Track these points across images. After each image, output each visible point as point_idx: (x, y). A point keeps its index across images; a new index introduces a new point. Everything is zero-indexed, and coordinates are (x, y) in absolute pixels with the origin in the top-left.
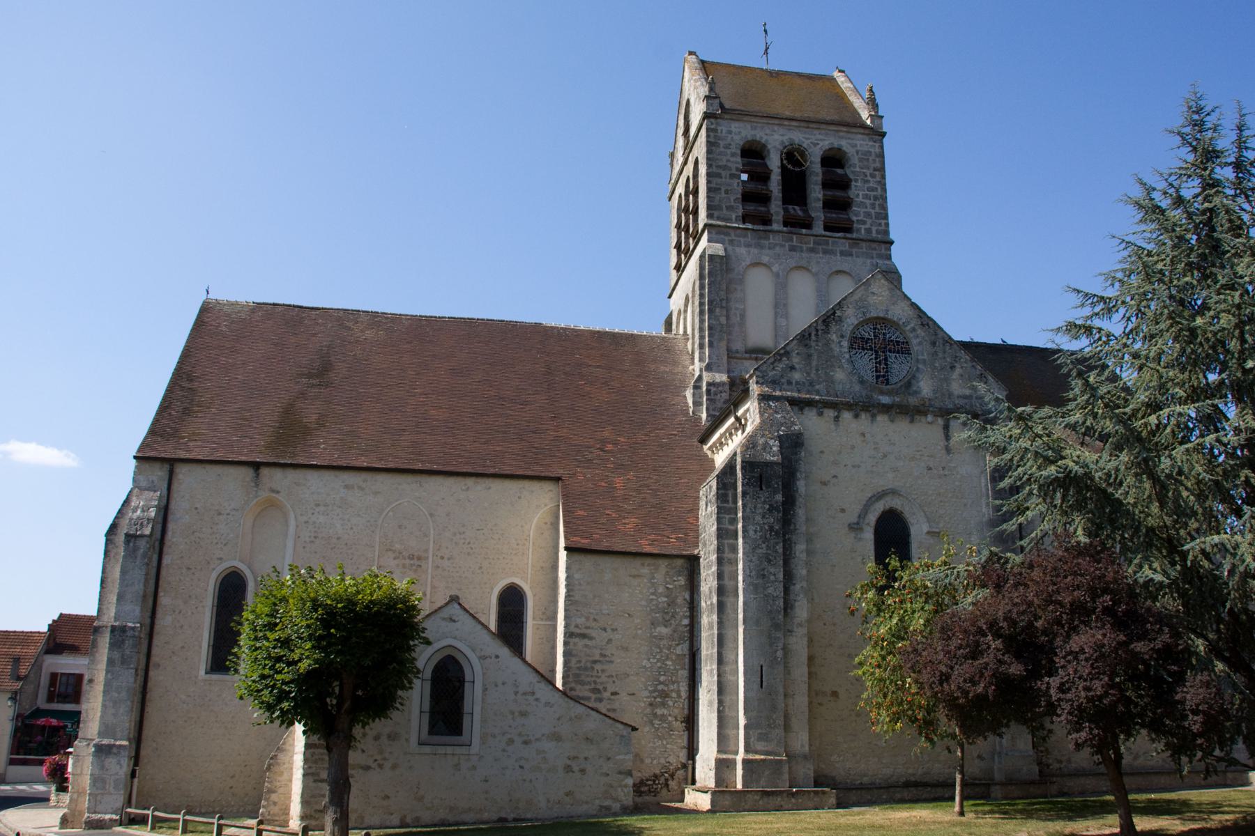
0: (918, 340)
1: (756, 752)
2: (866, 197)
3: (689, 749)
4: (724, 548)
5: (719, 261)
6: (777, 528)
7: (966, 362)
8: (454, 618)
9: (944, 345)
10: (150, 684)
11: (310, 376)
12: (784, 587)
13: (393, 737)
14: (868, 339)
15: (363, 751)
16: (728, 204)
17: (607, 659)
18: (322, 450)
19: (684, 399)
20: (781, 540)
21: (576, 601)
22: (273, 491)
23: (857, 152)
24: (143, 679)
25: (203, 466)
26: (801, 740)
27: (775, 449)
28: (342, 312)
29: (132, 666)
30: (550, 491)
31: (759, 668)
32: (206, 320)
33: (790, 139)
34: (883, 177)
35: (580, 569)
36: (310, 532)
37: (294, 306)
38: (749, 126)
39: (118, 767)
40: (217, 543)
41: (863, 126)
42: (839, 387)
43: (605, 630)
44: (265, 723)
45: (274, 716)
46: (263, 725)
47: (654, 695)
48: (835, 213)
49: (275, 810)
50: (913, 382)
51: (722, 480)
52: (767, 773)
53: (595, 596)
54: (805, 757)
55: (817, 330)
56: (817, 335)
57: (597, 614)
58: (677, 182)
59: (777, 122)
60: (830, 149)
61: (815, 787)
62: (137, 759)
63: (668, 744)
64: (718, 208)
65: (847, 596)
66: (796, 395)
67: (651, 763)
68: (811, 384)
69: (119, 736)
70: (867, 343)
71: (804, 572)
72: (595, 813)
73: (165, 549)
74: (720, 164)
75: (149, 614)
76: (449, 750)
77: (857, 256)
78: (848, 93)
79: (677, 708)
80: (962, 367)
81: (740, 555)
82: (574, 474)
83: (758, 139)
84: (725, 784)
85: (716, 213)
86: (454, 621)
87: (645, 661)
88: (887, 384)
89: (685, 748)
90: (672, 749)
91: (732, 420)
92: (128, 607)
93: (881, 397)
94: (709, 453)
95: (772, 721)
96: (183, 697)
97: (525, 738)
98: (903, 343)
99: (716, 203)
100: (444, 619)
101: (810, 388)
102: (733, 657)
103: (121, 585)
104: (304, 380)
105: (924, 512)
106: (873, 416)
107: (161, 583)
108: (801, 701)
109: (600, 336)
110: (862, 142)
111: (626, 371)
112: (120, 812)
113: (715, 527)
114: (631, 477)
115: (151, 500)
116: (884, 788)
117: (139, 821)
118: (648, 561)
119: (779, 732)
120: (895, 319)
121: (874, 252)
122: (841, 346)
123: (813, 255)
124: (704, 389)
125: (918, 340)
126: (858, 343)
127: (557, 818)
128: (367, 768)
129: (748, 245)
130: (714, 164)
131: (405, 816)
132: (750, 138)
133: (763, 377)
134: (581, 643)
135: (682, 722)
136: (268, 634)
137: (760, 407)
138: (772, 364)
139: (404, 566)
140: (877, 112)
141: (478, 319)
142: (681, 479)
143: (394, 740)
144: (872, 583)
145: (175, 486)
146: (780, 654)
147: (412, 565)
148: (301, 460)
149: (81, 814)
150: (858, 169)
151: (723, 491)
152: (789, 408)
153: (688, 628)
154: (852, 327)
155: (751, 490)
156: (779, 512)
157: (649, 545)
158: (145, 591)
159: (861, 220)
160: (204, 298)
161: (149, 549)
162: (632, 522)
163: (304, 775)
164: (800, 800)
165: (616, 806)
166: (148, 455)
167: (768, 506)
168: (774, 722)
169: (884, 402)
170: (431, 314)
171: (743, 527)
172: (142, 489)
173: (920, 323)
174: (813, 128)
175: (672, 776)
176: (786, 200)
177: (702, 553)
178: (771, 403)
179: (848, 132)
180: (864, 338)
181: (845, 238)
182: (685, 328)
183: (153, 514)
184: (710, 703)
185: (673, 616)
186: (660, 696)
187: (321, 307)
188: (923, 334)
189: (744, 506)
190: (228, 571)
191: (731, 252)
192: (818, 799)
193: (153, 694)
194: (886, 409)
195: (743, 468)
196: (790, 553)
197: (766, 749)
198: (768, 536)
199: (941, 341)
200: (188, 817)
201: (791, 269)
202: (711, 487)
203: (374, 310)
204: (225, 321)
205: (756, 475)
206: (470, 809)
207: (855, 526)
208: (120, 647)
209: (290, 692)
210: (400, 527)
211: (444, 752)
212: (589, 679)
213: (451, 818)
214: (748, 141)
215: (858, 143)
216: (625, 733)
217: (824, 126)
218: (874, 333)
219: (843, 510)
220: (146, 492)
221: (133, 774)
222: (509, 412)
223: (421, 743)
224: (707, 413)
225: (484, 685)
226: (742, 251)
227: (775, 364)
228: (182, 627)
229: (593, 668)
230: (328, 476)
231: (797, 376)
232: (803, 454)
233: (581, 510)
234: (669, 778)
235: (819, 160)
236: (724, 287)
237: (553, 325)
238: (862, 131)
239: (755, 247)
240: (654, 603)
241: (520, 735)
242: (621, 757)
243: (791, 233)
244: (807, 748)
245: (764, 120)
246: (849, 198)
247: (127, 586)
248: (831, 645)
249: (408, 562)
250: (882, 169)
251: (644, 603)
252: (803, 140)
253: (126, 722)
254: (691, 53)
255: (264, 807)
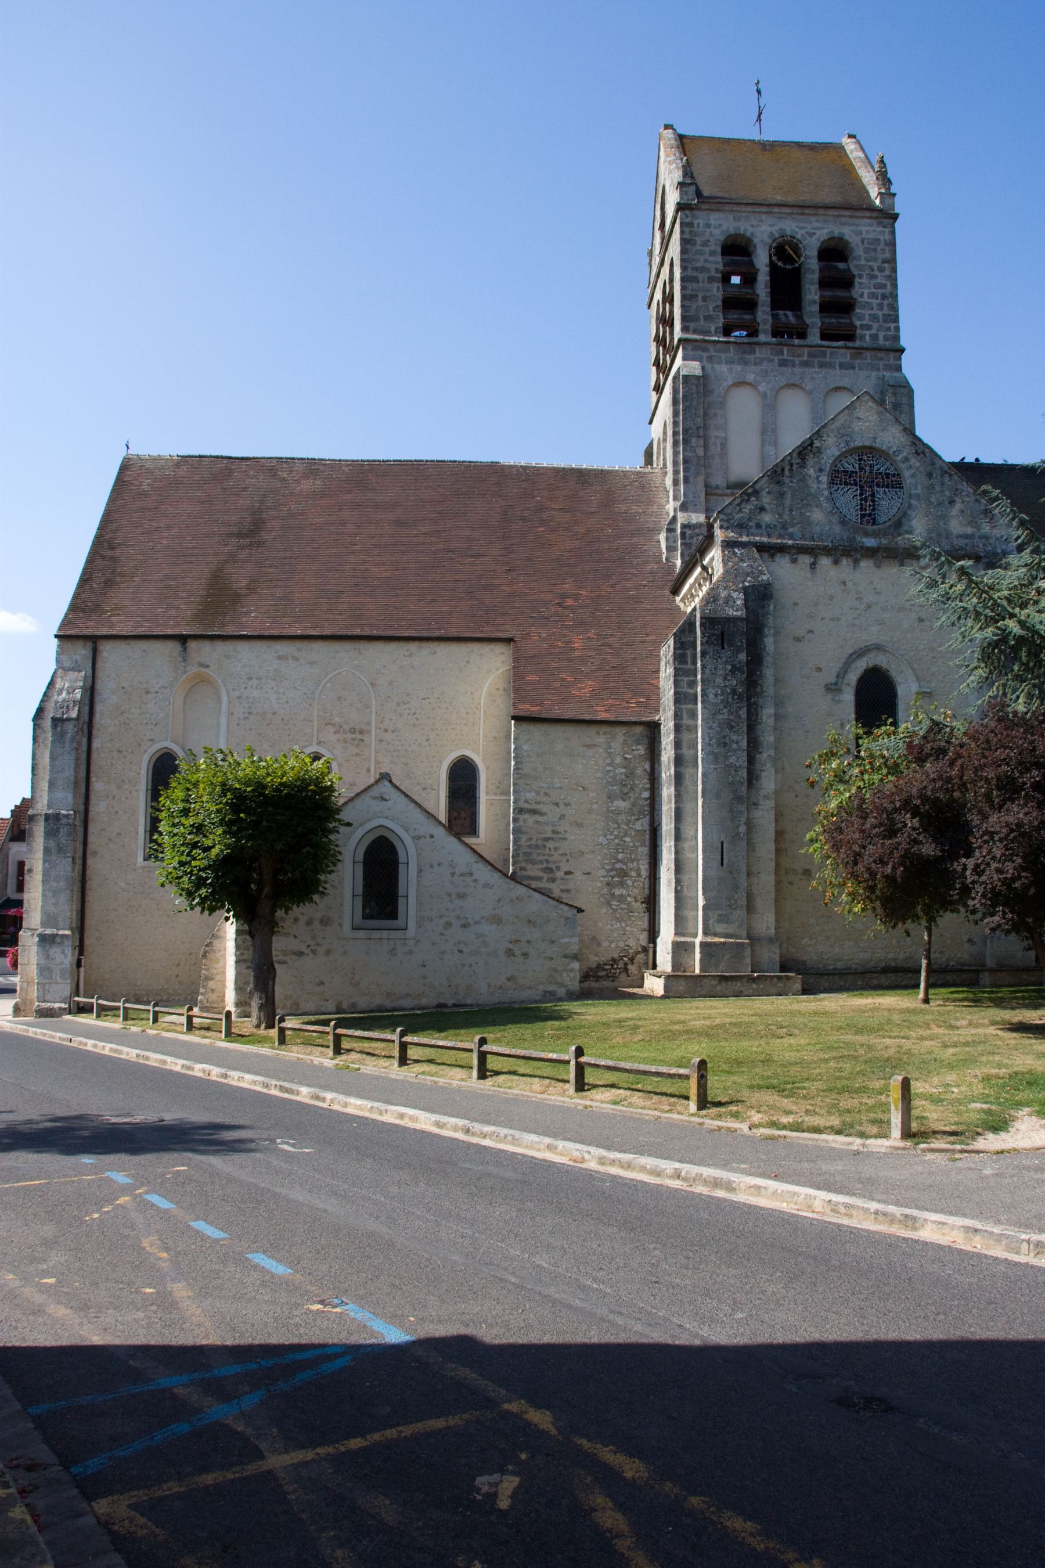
0: (911, 471)
1: (716, 935)
2: (872, 295)
3: (649, 931)
4: (682, 714)
5: (695, 382)
6: (740, 690)
7: (968, 496)
8: (385, 796)
9: (942, 476)
10: (88, 872)
11: (240, 536)
12: (749, 755)
13: (325, 922)
14: (852, 472)
15: (295, 937)
16: (706, 314)
17: (560, 836)
18: (253, 620)
19: (656, 544)
20: (745, 704)
21: (525, 775)
22: (201, 665)
23: (863, 242)
24: (81, 867)
25: (128, 642)
26: (766, 922)
27: (739, 602)
28: (275, 461)
29: (69, 855)
30: (502, 653)
31: (720, 846)
32: (126, 479)
33: (780, 229)
34: (894, 270)
35: (529, 740)
36: (244, 707)
37: (222, 457)
38: (731, 217)
39: (63, 956)
40: (147, 724)
41: (871, 208)
42: (816, 530)
43: (557, 805)
44: (186, 910)
45: (194, 903)
46: (183, 912)
47: (612, 874)
48: (837, 318)
49: (213, 997)
50: (904, 520)
51: (680, 638)
52: (727, 957)
53: (546, 769)
54: (771, 940)
55: (791, 465)
56: (791, 470)
57: (548, 788)
58: (655, 286)
59: (764, 209)
60: (829, 239)
61: (781, 972)
62: (81, 949)
63: (627, 926)
64: (695, 319)
65: (807, 766)
66: (765, 540)
67: (609, 946)
68: (784, 527)
69: (61, 924)
70: (850, 477)
71: (772, 739)
72: (538, 998)
73: (94, 732)
74: (697, 265)
75: (82, 801)
76: (385, 934)
77: (860, 369)
78: (857, 165)
79: (637, 888)
80: (963, 502)
81: (700, 721)
82: (528, 634)
83: (742, 232)
84: (683, 969)
85: (692, 325)
86: (385, 800)
87: (601, 838)
88: (874, 523)
89: (645, 930)
90: (632, 932)
91: (699, 570)
92: (60, 794)
93: (864, 540)
94: (681, 605)
95: (733, 902)
96: (123, 885)
97: (463, 921)
98: (894, 475)
99: (692, 313)
100: (374, 798)
101: (782, 532)
102: (692, 833)
103: (51, 771)
104: (234, 541)
105: (913, 670)
106: (856, 562)
107: (92, 768)
108: (766, 880)
109: (565, 474)
110: (868, 228)
111: (592, 513)
112: (68, 1000)
113: (672, 691)
114: (592, 636)
115: (76, 681)
116: (859, 973)
117: (83, 1009)
118: (605, 729)
119: (740, 913)
120: (884, 448)
121: (881, 363)
122: (819, 482)
123: (806, 369)
124: (679, 531)
125: (911, 471)
126: (839, 477)
127: (499, 1003)
128: (301, 954)
129: (730, 362)
130: (690, 266)
131: (341, 1002)
132: (732, 231)
133: (728, 521)
134: (531, 819)
135: (642, 903)
136: (183, 820)
137: (724, 556)
138: (739, 505)
139: (345, 741)
140: (889, 189)
141: (427, 461)
142: (647, 635)
143: (326, 925)
144: (832, 752)
145: (100, 664)
146: (742, 829)
147: (354, 739)
148: (230, 631)
149: (32, 1003)
150: (863, 262)
151: (681, 651)
152: (757, 555)
153: (649, 801)
154: (833, 459)
155: (710, 650)
156: (742, 673)
157: (606, 711)
158: (76, 777)
159: (866, 325)
160: (123, 453)
161: (77, 733)
162: (589, 686)
163: (237, 962)
164: (762, 986)
165: (561, 992)
166: (69, 633)
167: (729, 667)
168: (736, 902)
169: (868, 545)
170: (374, 458)
171: (702, 690)
172: (66, 670)
173: (914, 451)
174: (808, 214)
175: (632, 960)
176: (776, 304)
177: (662, 719)
178: (736, 550)
179: (851, 217)
180: (847, 472)
181: (847, 348)
182: (665, 459)
183: (79, 696)
184: (669, 882)
185: (632, 789)
186: (618, 875)
187: (251, 456)
188: (918, 464)
189: (703, 667)
190: (162, 752)
191: (709, 372)
192: (782, 985)
193: (92, 883)
194: (871, 553)
195: (702, 625)
196: (757, 718)
197: (726, 931)
198: (730, 699)
199: (939, 472)
200: (127, 1005)
201: (781, 388)
202: (669, 646)
203: (310, 457)
204: (148, 478)
205: (717, 632)
206: (408, 995)
207: (833, 687)
208: (55, 835)
209: (207, 878)
210: (339, 698)
211: (378, 936)
212: (540, 858)
213: (388, 1004)
214: (730, 235)
215: (864, 229)
216: (570, 915)
217: (821, 211)
218: (859, 464)
219: (819, 670)
220: (71, 672)
221: (79, 964)
222: (459, 566)
223: (355, 928)
224: (682, 559)
225: (418, 866)
226: (723, 368)
227: (742, 506)
228: (116, 813)
229: (544, 846)
230: (260, 646)
231: (767, 518)
232: (772, 607)
233: (532, 675)
234: (629, 962)
235: (816, 253)
236: (701, 412)
237: (512, 463)
238: (868, 214)
239: (739, 364)
240: (611, 774)
241: (458, 917)
242: (566, 940)
243: (781, 344)
244: (773, 931)
245: (750, 209)
246: (852, 298)
247: (58, 772)
248: (803, 819)
249: (349, 736)
250: (892, 261)
251: (599, 775)
252: (797, 230)
253: (67, 910)
254: (667, 127)
255: (202, 994)
